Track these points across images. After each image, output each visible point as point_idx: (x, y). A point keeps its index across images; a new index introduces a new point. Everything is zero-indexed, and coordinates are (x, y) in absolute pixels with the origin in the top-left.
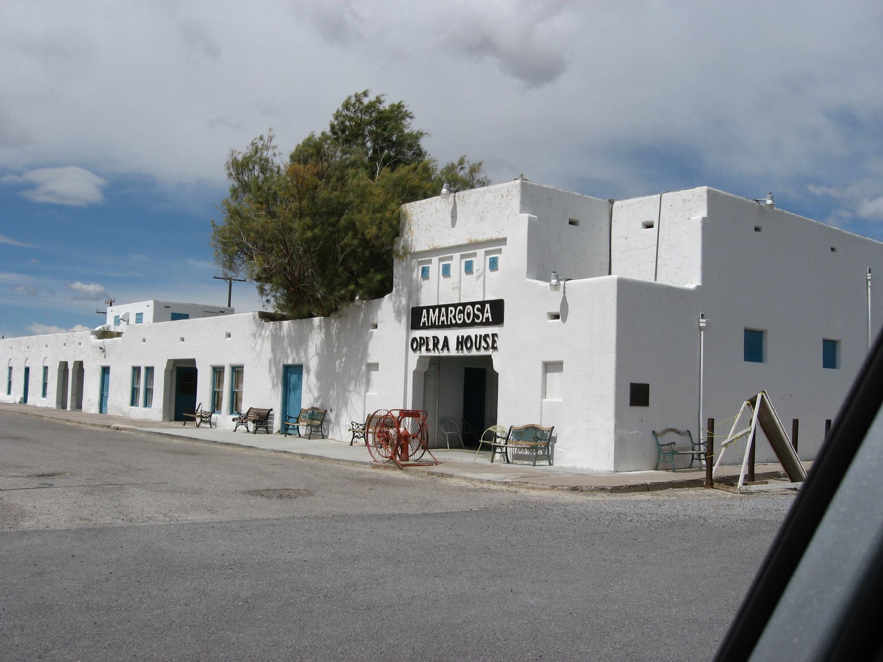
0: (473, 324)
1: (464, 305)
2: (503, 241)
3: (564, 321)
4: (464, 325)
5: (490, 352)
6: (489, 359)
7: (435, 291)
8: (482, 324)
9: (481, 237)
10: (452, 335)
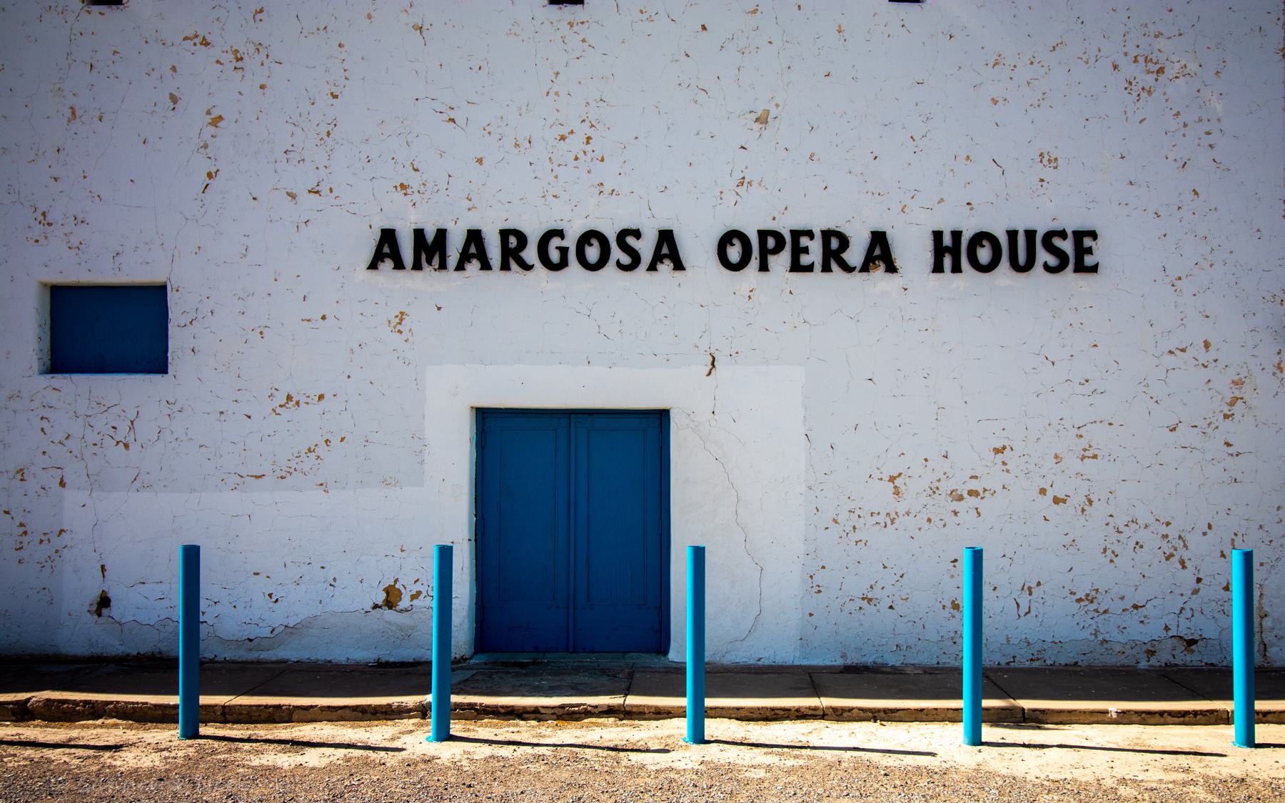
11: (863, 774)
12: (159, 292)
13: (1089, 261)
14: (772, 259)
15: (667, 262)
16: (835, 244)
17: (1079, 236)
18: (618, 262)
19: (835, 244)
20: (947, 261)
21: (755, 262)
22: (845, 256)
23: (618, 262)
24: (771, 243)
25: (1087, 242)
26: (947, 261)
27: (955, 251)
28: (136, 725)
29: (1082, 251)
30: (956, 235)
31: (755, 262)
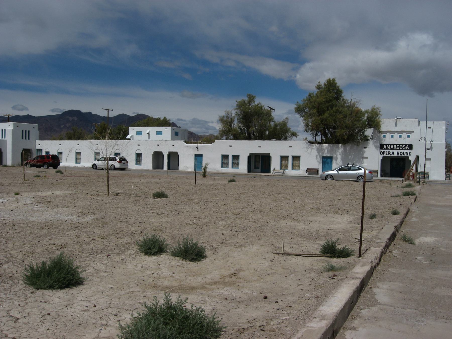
0: (403, 149)
1: (400, 145)
2: (413, 132)
3: (431, 150)
4: (400, 149)
5: (408, 156)
6: (408, 157)
7: (388, 140)
8: (405, 149)
9: (405, 130)
10: (395, 152)
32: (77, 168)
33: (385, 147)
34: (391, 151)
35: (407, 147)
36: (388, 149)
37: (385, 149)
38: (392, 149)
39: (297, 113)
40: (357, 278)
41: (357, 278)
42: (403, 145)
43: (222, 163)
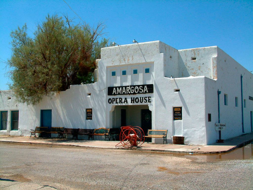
4: (134, 93)
6: (147, 106)
11: (186, 80)
12: (50, 111)
13: (150, 101)
14: (114, 102)
15: (126, 102)
16: (121, 100)
17: (149, 97)
18: (144, 101)
19: (121, 100)
20: (133, 102)
21: (112, 103)
22: (122, 101)
23: (144, 101)
24: (114, 100)
25: (150, 98)
26: (133, 102)
27: (134, 100)
28: (215, 65)
29: (149, 100)
30: (134, 98)
31: (112, 103)
32: (183, 106)
33: (114, 91)
34: (123, 97)
35: (146, 88)
36: (119, 94)
37: (114, 94)
38: (124, 94)
39: (13, 53)
40: (178, 87)
41: (178, 87)
42: (139, 86)
43: (91, 113)
